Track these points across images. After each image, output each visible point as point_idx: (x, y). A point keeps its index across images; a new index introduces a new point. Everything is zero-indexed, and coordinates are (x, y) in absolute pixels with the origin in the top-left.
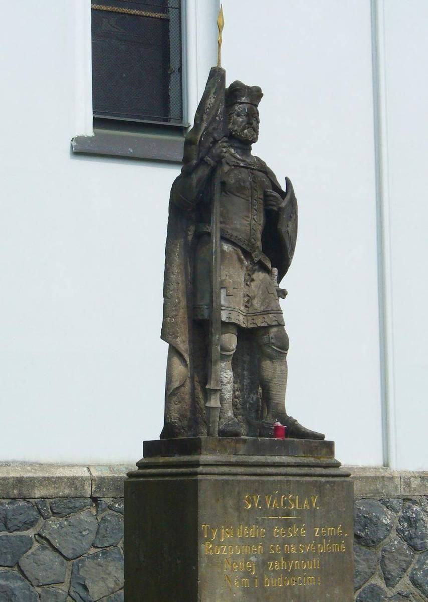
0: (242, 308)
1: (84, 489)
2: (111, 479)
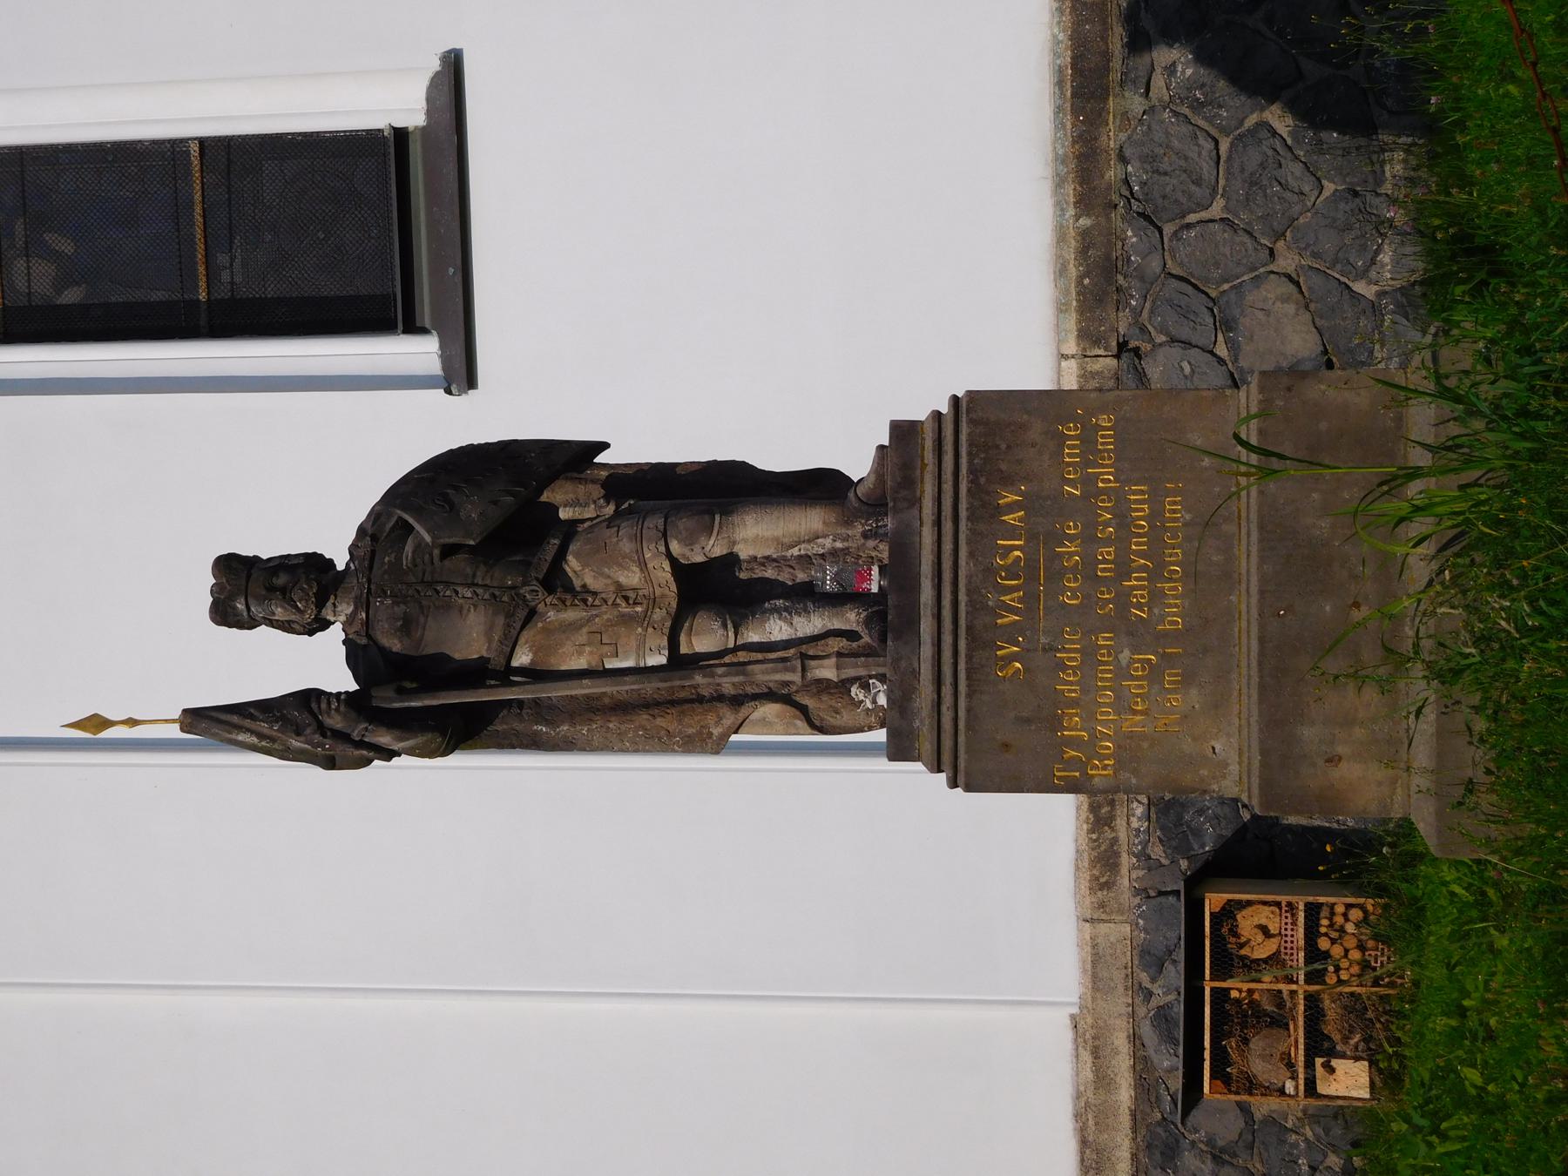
1: (1102, 372)
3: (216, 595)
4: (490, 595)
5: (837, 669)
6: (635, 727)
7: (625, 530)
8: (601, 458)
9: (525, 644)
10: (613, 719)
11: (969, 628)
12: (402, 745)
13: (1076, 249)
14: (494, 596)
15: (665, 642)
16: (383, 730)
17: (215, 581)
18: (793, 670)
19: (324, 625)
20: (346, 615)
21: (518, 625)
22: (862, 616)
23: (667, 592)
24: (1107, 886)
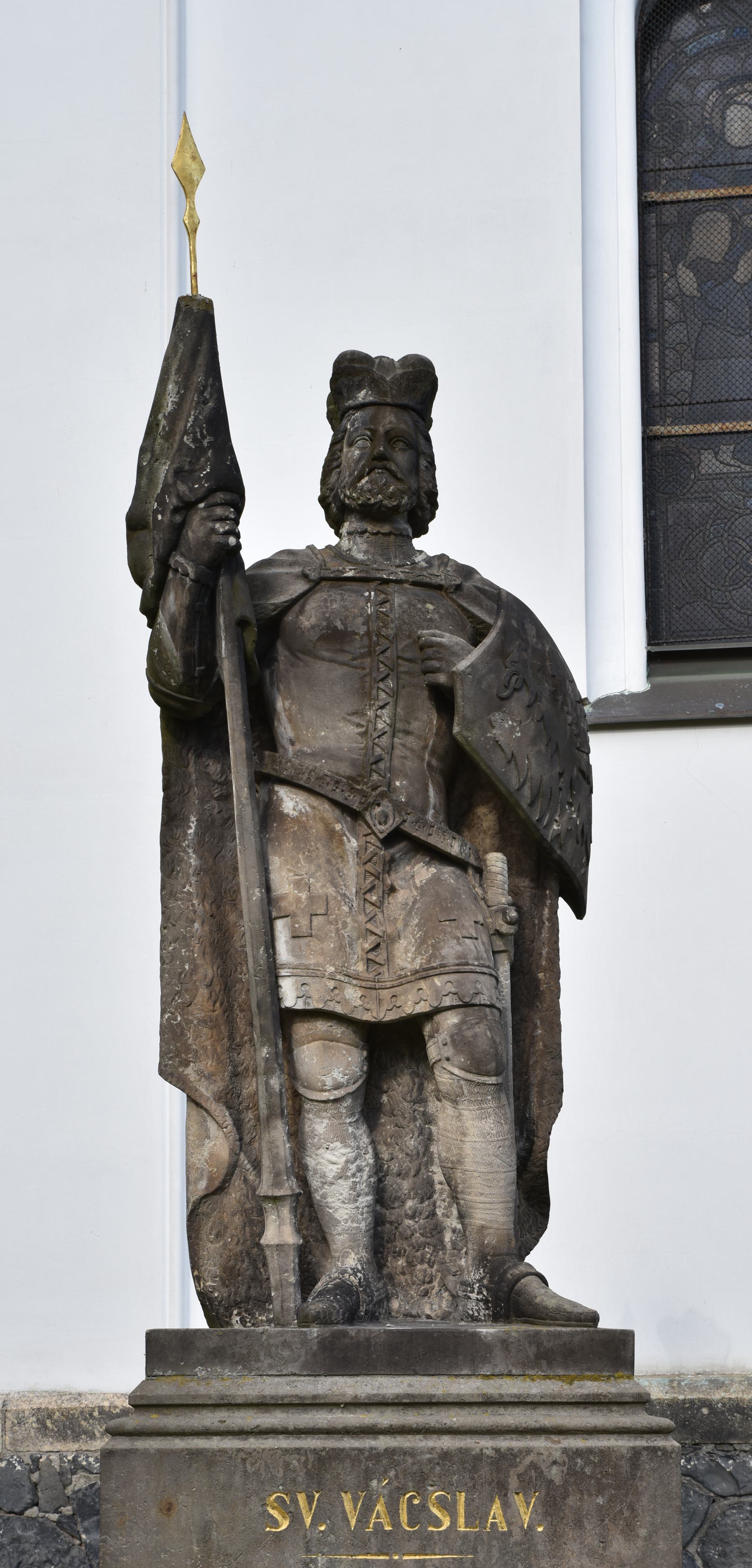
0: (361, 967)
2: (669, 1405)
3: (377, 361)
4: (380, 755)
5: (277, 1245)
6: (194, 959)
7: (473, 947)
8: (564, 909)
9: (310, 805)
10: (207, 928)
11: (336, 1455)
12: (165, 627)
13: (742, 1400)
14: (379, 760)
15: (315, 1004)
16: (185, 599)
17: (396, 359)
18: (277, 1184)
19: (335, 522)
20: (350, 550)
21: (338, 796)
22: (352, 1278)
23: (386, 1006)
24: (43, 1428)
